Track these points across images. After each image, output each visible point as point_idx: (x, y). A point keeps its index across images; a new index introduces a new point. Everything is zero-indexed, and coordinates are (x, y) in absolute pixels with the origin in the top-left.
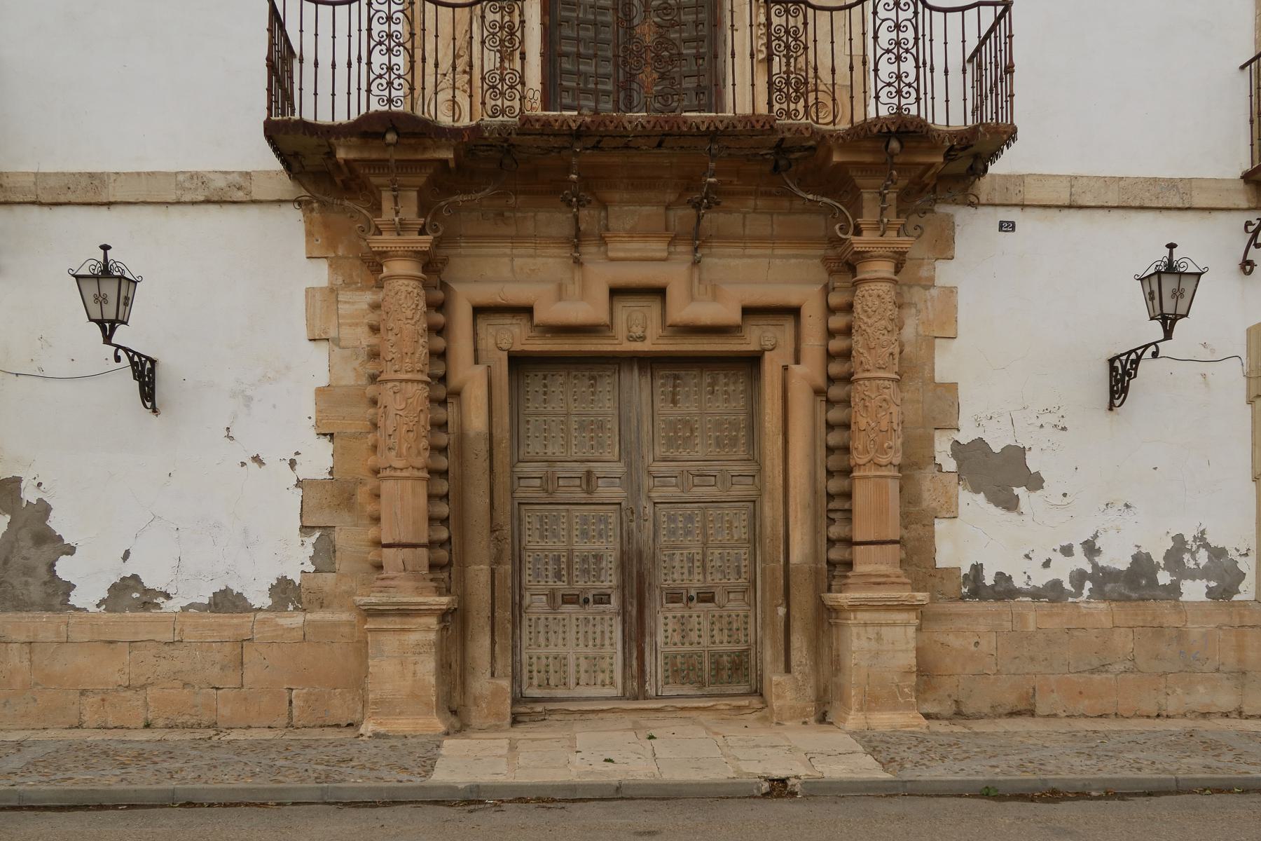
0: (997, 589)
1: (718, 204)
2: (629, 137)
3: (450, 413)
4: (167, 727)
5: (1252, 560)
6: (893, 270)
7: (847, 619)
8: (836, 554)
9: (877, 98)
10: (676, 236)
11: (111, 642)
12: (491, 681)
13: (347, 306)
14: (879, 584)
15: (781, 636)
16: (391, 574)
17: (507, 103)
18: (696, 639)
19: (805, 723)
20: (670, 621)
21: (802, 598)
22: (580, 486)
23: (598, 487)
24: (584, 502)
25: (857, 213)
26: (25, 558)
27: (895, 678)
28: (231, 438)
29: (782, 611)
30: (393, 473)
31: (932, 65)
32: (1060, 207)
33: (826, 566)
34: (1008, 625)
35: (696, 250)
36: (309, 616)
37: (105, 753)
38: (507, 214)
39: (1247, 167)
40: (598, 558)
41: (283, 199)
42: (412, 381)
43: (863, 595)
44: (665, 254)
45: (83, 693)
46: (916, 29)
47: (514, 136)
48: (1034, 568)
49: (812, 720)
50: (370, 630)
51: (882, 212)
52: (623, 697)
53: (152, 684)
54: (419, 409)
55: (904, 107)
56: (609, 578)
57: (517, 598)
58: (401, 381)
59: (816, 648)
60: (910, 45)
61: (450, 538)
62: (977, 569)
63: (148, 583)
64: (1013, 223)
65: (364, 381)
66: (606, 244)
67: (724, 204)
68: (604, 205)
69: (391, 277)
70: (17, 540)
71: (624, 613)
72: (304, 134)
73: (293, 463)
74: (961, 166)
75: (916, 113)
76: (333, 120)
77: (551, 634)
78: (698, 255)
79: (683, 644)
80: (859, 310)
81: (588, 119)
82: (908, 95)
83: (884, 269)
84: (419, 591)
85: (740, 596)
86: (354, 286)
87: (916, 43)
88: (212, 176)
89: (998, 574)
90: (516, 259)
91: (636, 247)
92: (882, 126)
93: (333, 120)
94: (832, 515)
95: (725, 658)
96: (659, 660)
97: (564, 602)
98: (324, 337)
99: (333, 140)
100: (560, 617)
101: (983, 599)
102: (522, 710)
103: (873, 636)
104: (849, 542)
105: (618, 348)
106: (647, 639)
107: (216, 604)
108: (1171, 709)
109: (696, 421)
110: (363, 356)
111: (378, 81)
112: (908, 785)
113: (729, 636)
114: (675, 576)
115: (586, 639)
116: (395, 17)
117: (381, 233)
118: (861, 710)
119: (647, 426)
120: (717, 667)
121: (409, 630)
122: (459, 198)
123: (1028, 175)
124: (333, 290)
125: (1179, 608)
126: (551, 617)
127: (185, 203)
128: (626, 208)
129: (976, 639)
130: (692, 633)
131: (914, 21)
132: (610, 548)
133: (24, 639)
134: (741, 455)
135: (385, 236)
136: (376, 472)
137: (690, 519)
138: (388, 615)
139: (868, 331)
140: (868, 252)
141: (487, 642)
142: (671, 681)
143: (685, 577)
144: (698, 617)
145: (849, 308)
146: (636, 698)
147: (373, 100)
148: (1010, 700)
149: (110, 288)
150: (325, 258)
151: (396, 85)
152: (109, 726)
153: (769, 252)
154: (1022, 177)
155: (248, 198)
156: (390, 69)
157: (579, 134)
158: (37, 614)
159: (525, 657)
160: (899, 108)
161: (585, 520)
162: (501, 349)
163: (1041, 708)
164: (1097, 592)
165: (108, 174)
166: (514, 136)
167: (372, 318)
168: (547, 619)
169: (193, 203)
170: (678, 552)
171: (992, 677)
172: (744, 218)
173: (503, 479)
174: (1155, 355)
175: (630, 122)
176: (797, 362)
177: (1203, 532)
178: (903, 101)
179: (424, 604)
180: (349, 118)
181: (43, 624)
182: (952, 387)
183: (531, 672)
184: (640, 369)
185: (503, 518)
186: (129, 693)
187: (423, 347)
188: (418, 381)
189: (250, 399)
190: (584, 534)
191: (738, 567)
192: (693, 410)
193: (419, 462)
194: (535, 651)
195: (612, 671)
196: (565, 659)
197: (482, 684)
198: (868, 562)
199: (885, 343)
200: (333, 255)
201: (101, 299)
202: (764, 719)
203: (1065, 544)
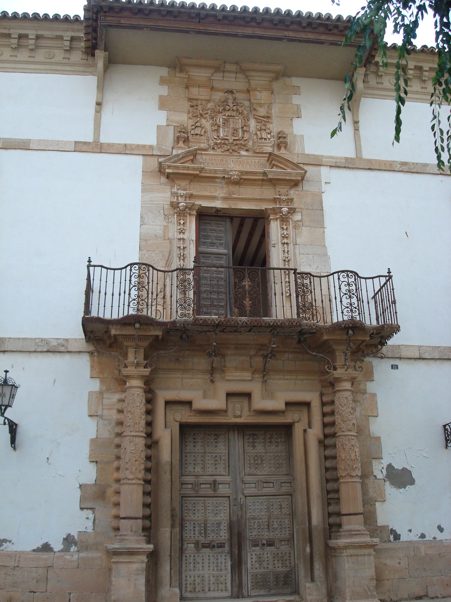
1: (275, 356)
2: (238, 327)
6: (351, 386)
7: (342, 553)
8: (333, 520)
9: (342, 312)
10: (255, 370)
12: (170, 589)
13: (107, 400)
14: (356, 535)
16: (124, 533)
17: (187, 312)
20: (254, 556)
22: (211, 488)
23: (219, 488)
24: (213, 496)
25: (334, 360)
27: (366, 582)
29: (308, 550)
30: (128, 481)
31: (362, 300)
33: (328, 527)
35: (264, 376)
38: (180, 359)
40: (219, 524)
41: (82, 351)
44: (250, 378)
46: (356, 285)
47: (190, 326)
51: (345, 360)
54: (141, 450)
55: (354, 317)
56: (224, 535)
58: (133, 436)
59: (326, 568)
60: (354, 292)
61: (151, 515)
64: (397, 365)
65: (113, 436)
67: (277, 356)
68: (223, 356)
72: (99, 323)
74: (377, 341)
75: (359, 319)
76: (111, 318)
78: (266, 379)
79: (260, 568)
80: (338, 404)
81: (223, 320)
82: (355, 312)
85: (286, 543)
86: (110, 391)
87: (356, 291)
88: (51, 340)
90: (184, 380)
91: (238, 375)
92: (346, 324)
93: (111, 318)
94: (329, 501)
96: (249, 576)
98: (95, 414)
104: (339, 514)
105: (230, 421)
106: (243, 567)
109: (264, 456)
110: (113, 424)
111: (133, 301)
113: (282, 564)
116: (141, 275)
117: (127, 368)
123: (401, 345)
124: (101, 393)
126: (196, 555)
127: (38, 352)
128: (233, 357)
129: (399, 561)
130: (264, 563)
131: (355, 282)
135: (129, 368)
136: (118, 481)
139: (343, 413)
140: (340, 378)
141: (168, 568)
144: (267, 554)
145: (333, 402)
147: (131, 310)
150: (99, 378)
151: (141, 304)
153: (294, 377)
155: (66, 350)
157: (217, 326)
160: (352, 317)
162: (176, 421)
165: (6, 338)
166: (190, 326)
168: (194, 556)
169: (41, 352)
170: (257, 521)
172: (283, 363)
175: (240, 321)
176: (310, 427)
179: (141, 548)
180: (118, 317)
183: (186, 584)
187: (144, 420)
188: (141, 436)
195: (226, 583)
196: (203, 577)
199: (350, 419)
200: (102, 376)
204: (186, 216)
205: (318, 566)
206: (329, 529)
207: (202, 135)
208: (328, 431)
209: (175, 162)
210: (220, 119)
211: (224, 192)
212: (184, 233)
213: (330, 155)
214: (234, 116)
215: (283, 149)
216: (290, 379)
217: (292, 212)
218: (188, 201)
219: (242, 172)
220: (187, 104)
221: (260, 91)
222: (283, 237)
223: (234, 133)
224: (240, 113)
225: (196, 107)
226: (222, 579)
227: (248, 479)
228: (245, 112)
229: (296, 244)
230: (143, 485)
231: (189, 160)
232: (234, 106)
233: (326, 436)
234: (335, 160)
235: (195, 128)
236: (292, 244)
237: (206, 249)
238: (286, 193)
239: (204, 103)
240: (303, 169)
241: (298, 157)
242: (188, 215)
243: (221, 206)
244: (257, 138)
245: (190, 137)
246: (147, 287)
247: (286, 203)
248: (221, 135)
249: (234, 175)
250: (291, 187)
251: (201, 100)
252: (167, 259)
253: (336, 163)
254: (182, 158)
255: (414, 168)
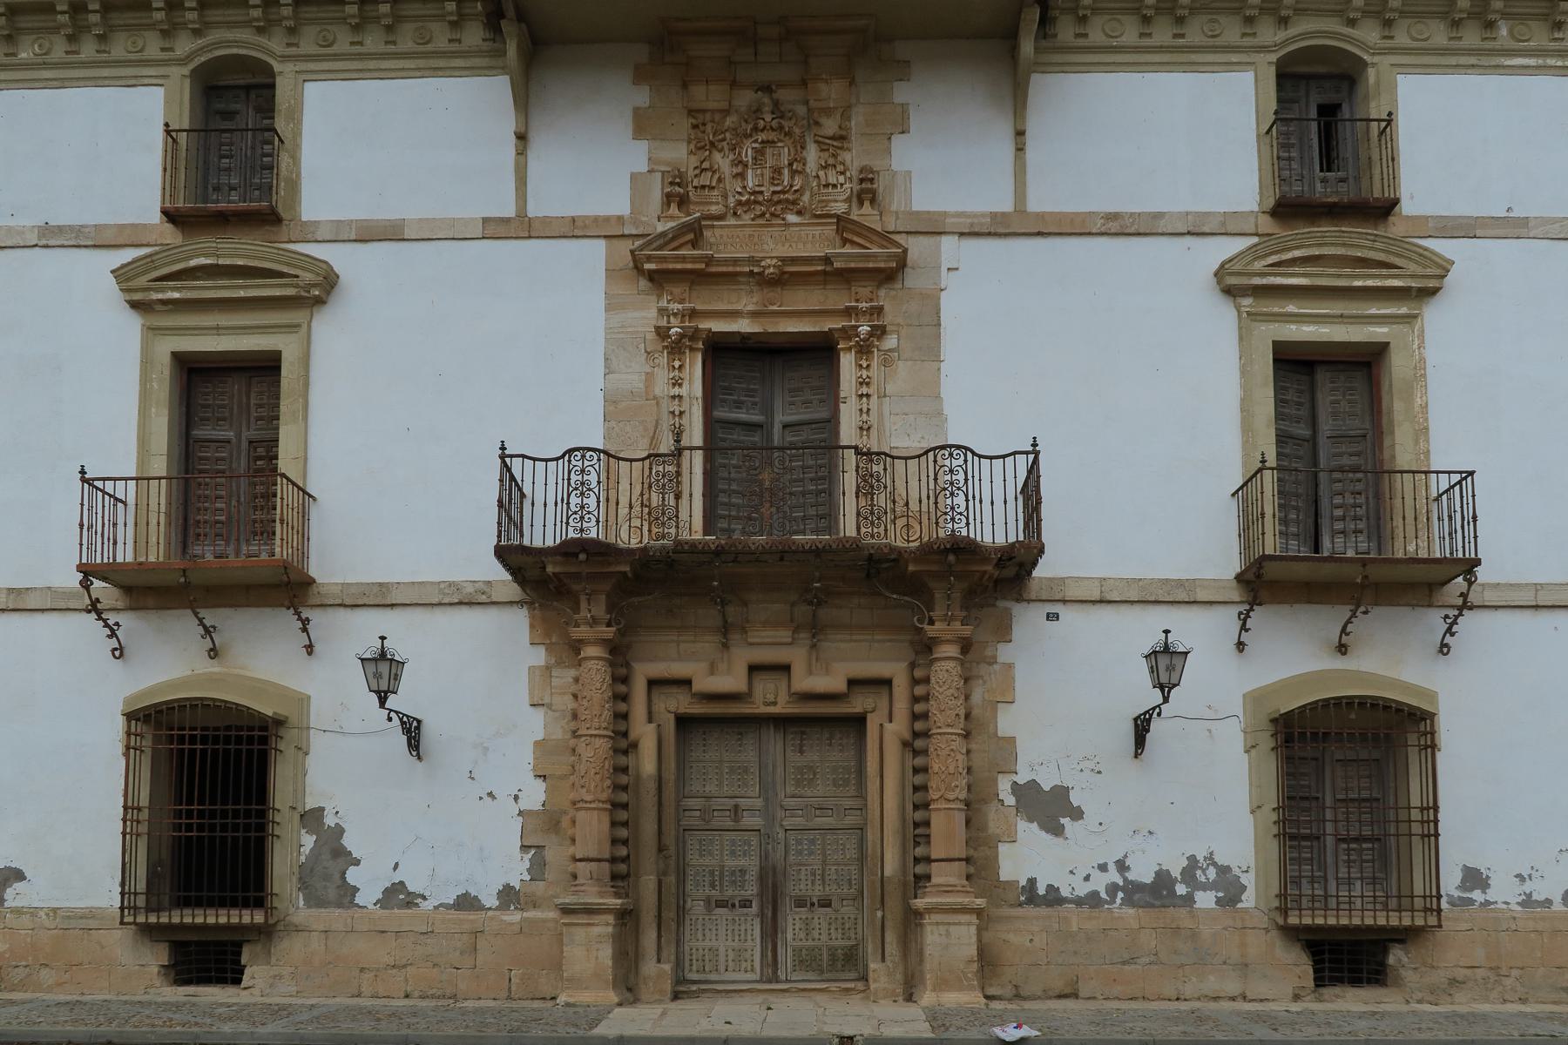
0: (1049, 897)
3: (630, 761)
4: (420, 997)
5: (1252, 874)
8: (920, 869)
11: (383, 932)
14: (948, 892)
15: (879, 933)
18: (817, 936)
19: (895, 1001)
20: (798, 922)
21: (894, 903)
25: (930, 608)
26: (325, 868)
28: (473, 779)
30: (585, 805)
32: (1094, 602)
34: (1056, 926)
35: (814, 636)
36: (525, 914)
37: (370, 1012)
39: (1238, 570)
42: (600, 736)
43: (934, 900)
44: (790, 640)
45: (362, 970)
48: (1077, 881)
49: (901, 998)
50: (565, 924)
52: (760, 981)
53: (411, 964)
57: (682, 902)
58: (591, 736)
61: (629, 855)
62: (1032, 882)
63: (411, 889)
65: (568, 736)
66: (746, 632)
68: (745, 604)
69: (585, 659)
70: (320, 854)
71: (762, 915)
73: (516, 798)
77: (707, 930)
83: (951, 650)
84: (601, 894)
85: (851, 902)
89: (1048, 886)
91: (769, 634)
94: (917, 840)
95: (839, 951)
97: (717, 906)
99: (543, 559)
100: (714, 918)
101: (1037, 905)
102: (681, 989)
103: (944, 933)
104: (928, 860)
105: (757, 711)
106: (779, 935)
107: (458, 905)
108: (1188, 995)
110: (569, 717)
111: (574, 516)
112: (945, 1042)
114: (802, 887)
115: (733, 935)
118: (934, 990)
119: (780, 770)
120: (833, 958)
121: (593, 925)
122: (635, 600)
124: (548, 668)
125: (1193, 914)
126: (707, 918)
127: (445, 604)
132: (752, 864)
133: (321, 928)
134: (852, 793)
135: (583, 628)
137: (813, 842)
138: (578, 913)
142: (797, 968)
143: (809, 887)
145: (927, 680)
146: (770, 982)
148: (1059, 985)
149: (384, 668)
152: (380, 995)
154: (1063, 579)
156: (582, 507)
158: (332, 910)
159: (687, 948)
160: (953, 531)
161: (733, 843)
162: (669, 712)
163: (1084, 991)
164: (1128, 901)
165: (392, 584)
167: (574, 688)
169: (451, 604)
171: (1044, 967)
173: (669, 811)
174: (1159, 714)
176: (891, 721)
177: (1211, 853)
178: (956, 526)
179: (604, 904)
181: (334, 917)
182: (1011, 741)
183: (691, 960)
184: (775, 727)
185: (670, 840)
186: (394, 971)
188: (604, 736)
189: (486, 749)
190: (733, 853)
191: (850, 880)
192: (816, 758)
193: (604, 796)
194: (694, 944)
197: (650, 967)
198: (943, 875)
201: (378, 676)
202: (867, 998)
203: (1101, 862)
204: (684, 353)
205: (891, 938)
206: (915, 882)
207: (713, 188)
208: (919, 726)
209: (660, 248)
210: (748, 154)
211: (755, 300)
212: (680, 385)
213: (960, 209)
214: (773, 142)
215: (867, 204)
216: (860, 641)
217: (879, 333)
218: (687, 324)
219: (784, 260)
220: (686, 123)
221: (826, 81)
222: (861, 384)
223: (773, 178)
224: (786, 135)
225: (702, 128)
226: (747, 955)
227: (790, 802)
228: (797, 131)
229: (885, 396)
230: (610, 810)
231: (687, 243)
232: (773, 119)
233: (916, 735)
234: (969, 221)
235: (701, 172)
236: (876, 396)
237: (728, 415)
238: (870, 296)
239: (717, 117)
240: (898, 245)
241: (897, 218)
242: (687, 351)
243: (749, 330)
244: (819, 186)
245: (690, 193)
246: (596, 490)
247: (868, 317)
248: (750, 185)
249: (769, 266)
250: (880, 285)
251: (713, 111)
252: (651, 434)
253: (972, 225)
254: (673, 239)
255: (1133, 224)
